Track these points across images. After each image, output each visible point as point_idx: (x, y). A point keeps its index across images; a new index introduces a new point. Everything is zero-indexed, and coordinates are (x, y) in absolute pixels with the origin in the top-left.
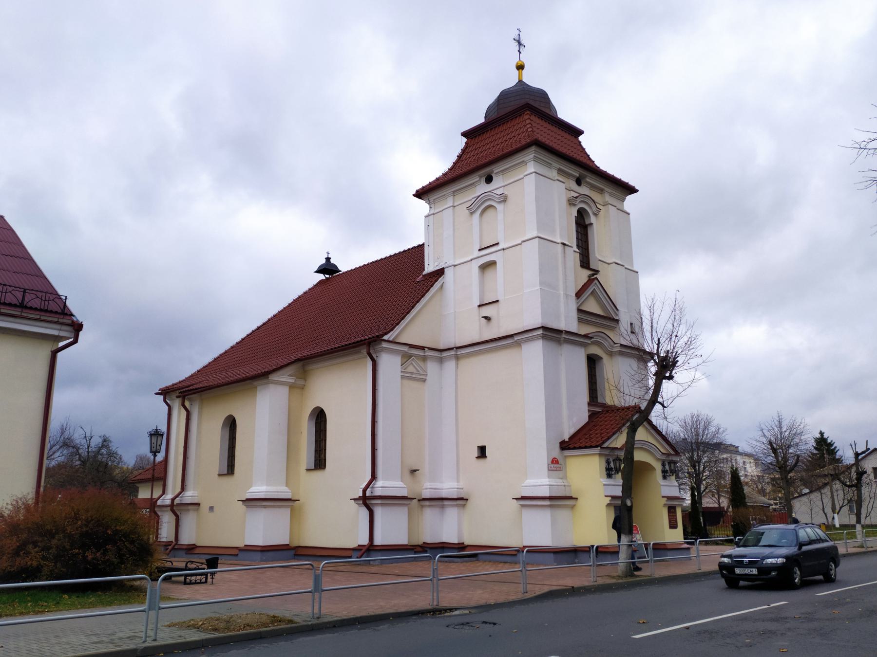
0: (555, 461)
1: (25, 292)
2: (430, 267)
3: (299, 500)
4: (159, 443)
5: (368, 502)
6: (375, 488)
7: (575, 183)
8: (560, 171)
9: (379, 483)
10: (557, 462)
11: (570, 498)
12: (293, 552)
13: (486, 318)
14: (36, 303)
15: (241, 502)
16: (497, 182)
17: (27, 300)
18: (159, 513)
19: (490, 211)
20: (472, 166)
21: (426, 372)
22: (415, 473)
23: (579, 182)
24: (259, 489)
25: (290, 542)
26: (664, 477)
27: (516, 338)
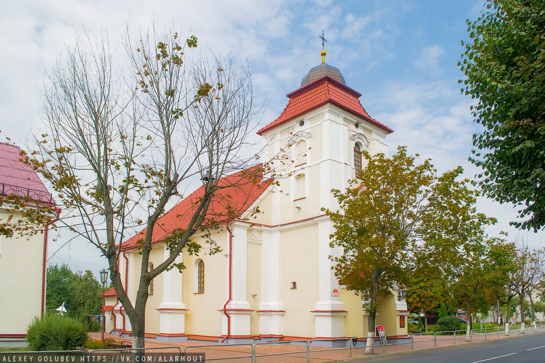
0: (335, 291)
1: (28, 191)
4: (106, 277)
5: (227, 312)
7: (354, 126)
8: (345, 119)
9: (232, 302)
10: (337, 291)
11: (344, 311)
12: (187, 338)
13: (298, 208)
14: (35, 197)
16: (307, 125)
17: (5, 191)
18: (116, 314)
19: (302, 143)
20: (292, 116)
23: (357, 125)
24: (166, 304)
25: (185, 332)
26: (399, 300)
27: (315, 220)
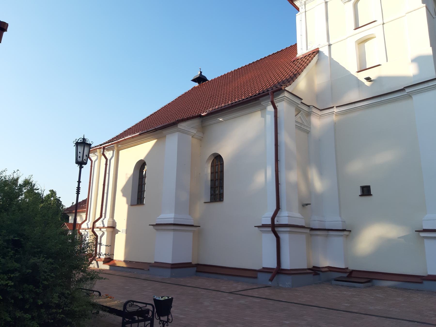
2: (301, 52)
3: (200, 226)
5: (276, 229)
6: (280, 217)
15: (152, 227)
21: (310, 126)
22: (307, 206)
27: (407, 90)
